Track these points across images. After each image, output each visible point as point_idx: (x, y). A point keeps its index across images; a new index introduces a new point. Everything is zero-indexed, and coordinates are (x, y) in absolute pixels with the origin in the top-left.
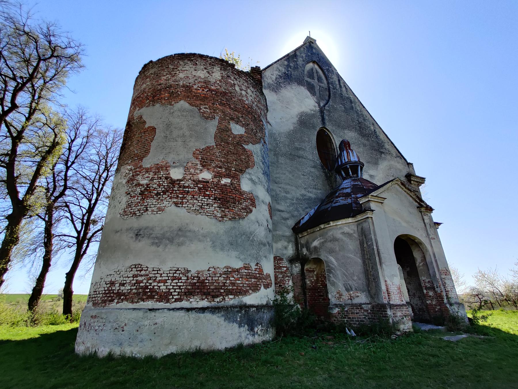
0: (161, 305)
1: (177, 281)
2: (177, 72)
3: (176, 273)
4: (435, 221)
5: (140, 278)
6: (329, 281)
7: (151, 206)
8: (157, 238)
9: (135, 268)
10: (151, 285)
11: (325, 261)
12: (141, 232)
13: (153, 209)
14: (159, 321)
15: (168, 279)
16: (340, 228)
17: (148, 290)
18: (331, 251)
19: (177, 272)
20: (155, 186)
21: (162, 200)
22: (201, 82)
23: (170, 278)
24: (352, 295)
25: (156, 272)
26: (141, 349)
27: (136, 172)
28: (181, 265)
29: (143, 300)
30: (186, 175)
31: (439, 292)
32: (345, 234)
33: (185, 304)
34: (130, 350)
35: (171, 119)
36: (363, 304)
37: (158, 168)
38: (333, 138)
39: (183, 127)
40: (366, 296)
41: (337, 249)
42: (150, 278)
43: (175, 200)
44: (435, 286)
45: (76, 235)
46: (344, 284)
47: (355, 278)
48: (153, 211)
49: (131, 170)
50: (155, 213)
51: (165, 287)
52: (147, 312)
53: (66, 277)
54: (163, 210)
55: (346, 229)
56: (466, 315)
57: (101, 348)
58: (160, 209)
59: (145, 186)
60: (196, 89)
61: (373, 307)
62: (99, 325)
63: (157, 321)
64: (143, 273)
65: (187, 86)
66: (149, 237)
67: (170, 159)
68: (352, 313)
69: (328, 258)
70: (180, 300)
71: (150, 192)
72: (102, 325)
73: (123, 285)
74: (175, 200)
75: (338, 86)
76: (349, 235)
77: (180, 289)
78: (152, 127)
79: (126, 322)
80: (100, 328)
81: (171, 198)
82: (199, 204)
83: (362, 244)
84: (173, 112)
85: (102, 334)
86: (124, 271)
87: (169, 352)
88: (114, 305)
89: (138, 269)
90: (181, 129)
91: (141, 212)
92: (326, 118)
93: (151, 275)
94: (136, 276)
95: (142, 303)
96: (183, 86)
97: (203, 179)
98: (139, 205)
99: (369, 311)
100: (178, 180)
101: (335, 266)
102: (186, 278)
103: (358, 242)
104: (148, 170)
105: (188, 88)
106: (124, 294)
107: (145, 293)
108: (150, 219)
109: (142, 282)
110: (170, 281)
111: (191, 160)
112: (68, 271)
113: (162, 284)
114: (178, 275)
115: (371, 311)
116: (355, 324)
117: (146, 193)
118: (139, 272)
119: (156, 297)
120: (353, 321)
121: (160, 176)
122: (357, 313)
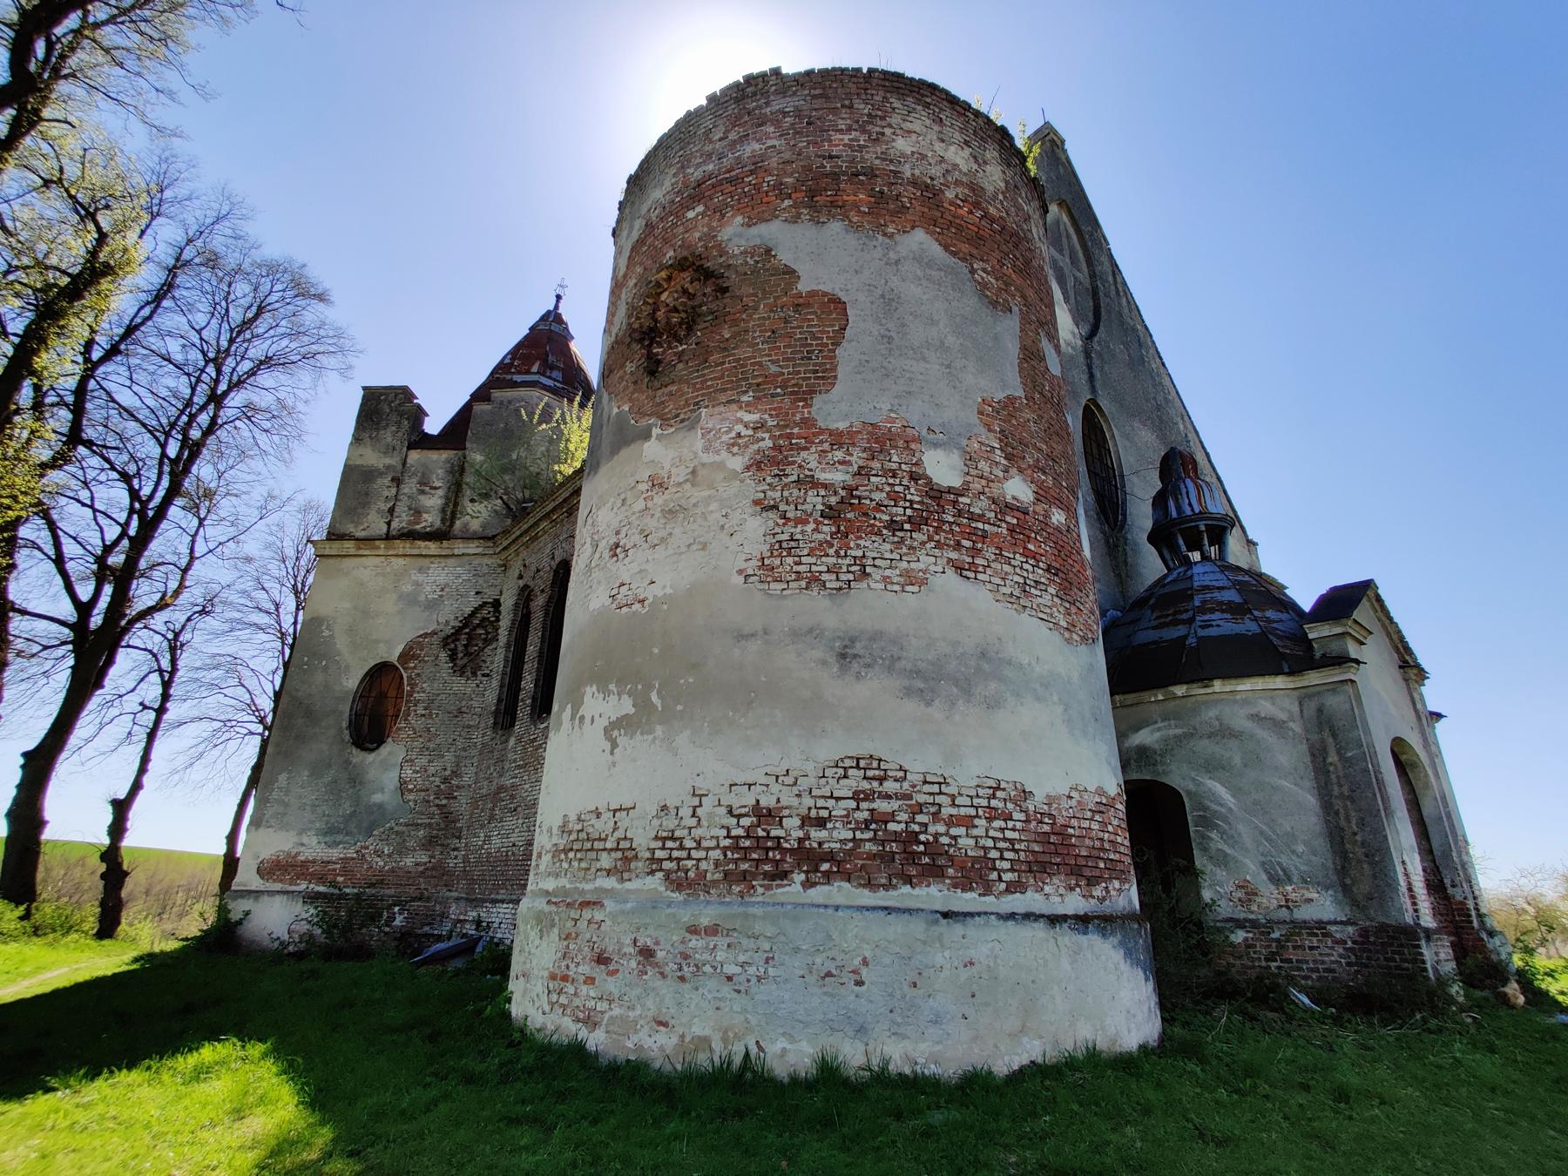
0: (968, 900)
1: (1003, 824)
2: (888, 131)
3: (994, 796)
4: (1431, 708)
5: (882, 806)
6: (1205, 850)
7: (878, 562)
8: (918, 673)
9: (858, 767)
10: (925, 832)
11: (1189, 793)
12: (858, 648)
13: (888, 573)
14: (980, 952)
15: (977, 816)
16: (1246, 702)
17: (922, 848)
18: (1213, 767)
19: (999, 794)
20: (878, 496)
21: (911, 548)
22: (962, 183)
23: (981, 812)
24: (1292, 896)
25: (936, 788)
26: (939, 1047)
27: (790, 436)
28: (1008, 773)
29: (908, 880)
30: (969, 478)
31: (1459, 898)
32: (1262, 719)
33: (1030, 900)
34: (903, 1052)
35: (895, 282)
36: (1329, 923)
37: (880, 440)
38: (1113, 436)
39: (936, 318)
40: (1337, 902)
41: (1237, 760)
42: (920, 808)
43: (954, 555)
44: (1447, 882)
45: (67, 610)
46: (1263, 863)
47: (1300, 848)
48: (885, 579)
49: (760, 426)
50: (897, 588)
51: (972, 842)
52: (936, 922)
53: (23, 767)
54: (923, 582)
55: (1266, 707)
56: (1509, 962)
57: (773, 1042)
58: (910, 579)
59: (843, 493)
60: (952, 203)
61: (1364, 933)
62: (742, 958)
63: (972, 953)
64: (890, 786)
65: (927, 186)
66: (890, 669)
67: (916, 414)
68: (1294, 948)
69: (1199, 784)
70: (1014, 888)
71: (866, 514)
72: (760, 958)
73: (821, 823)
74: (954, 555)
75: (1113, 293)
76: (1277, 725)
77: (1013, 850)
78: (825, 294)
79: (868, 954)
80: (752, 970)
81: (939, 545)
82: (1017, 578)
83: (1318, 755)
84: (897, 262)
85: (762, 992)
86: (812, 773)
87: (1024, 1060)
88: (793, 888)
89: (870, 773)
90: (933, 322)
91: (843, 577)
92: (1098, 375)
93: (922, 798)
94: (869, 796)
95: (907, 889)
96: (914, 182)
97: (1014, 498)
98: (831, 551)
99: (1350, 944)
100: (950, 490)
101: (1230, 810)
102: (1022, 817)
103: (1304, 747)
104: (839, 439)
105: (929, 193)
106: (830, 856)
107: (912, 857)
108: (875, 606)
109: (891, 817)
110: (983, 822)
111: (976, 430)
112: (31, 745)
113: (961, 831)
114: (1001, 805)
115: (1354, 942)
116: (1306, 978)
117: (845, 513)
118: (875, 784)
119: (951, 871)
120: (1300, 969)
121: (889, 465)
122: (1311, 948)
